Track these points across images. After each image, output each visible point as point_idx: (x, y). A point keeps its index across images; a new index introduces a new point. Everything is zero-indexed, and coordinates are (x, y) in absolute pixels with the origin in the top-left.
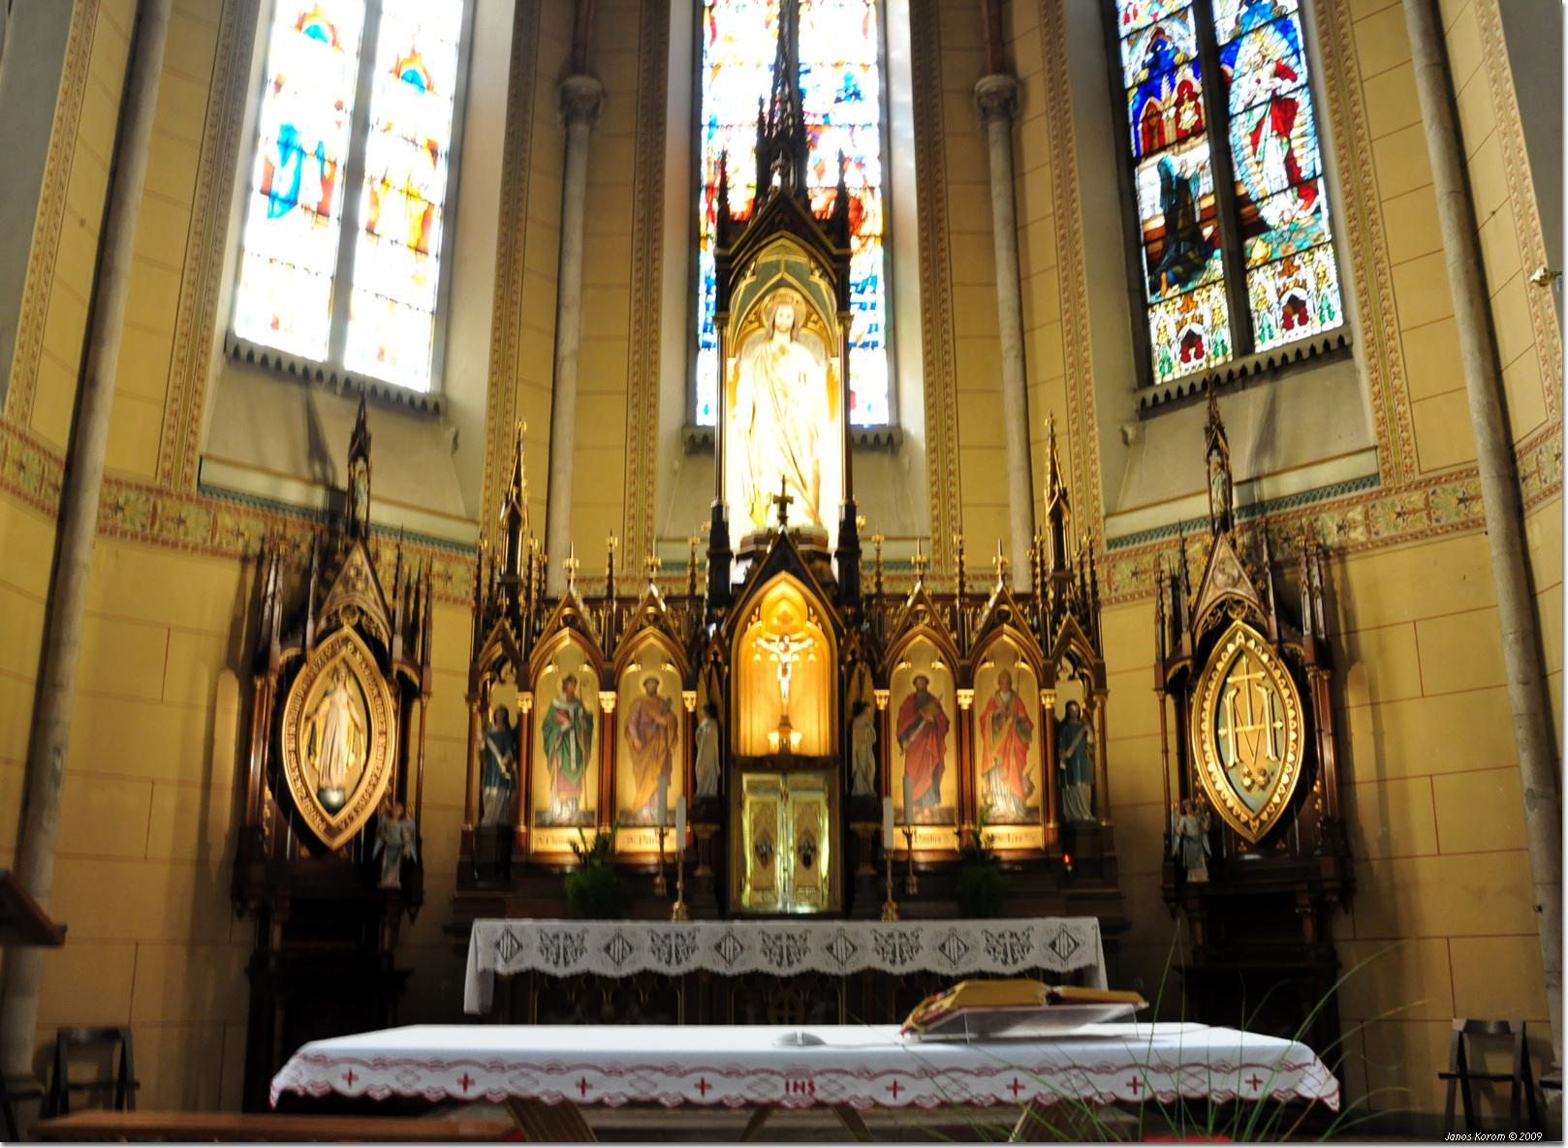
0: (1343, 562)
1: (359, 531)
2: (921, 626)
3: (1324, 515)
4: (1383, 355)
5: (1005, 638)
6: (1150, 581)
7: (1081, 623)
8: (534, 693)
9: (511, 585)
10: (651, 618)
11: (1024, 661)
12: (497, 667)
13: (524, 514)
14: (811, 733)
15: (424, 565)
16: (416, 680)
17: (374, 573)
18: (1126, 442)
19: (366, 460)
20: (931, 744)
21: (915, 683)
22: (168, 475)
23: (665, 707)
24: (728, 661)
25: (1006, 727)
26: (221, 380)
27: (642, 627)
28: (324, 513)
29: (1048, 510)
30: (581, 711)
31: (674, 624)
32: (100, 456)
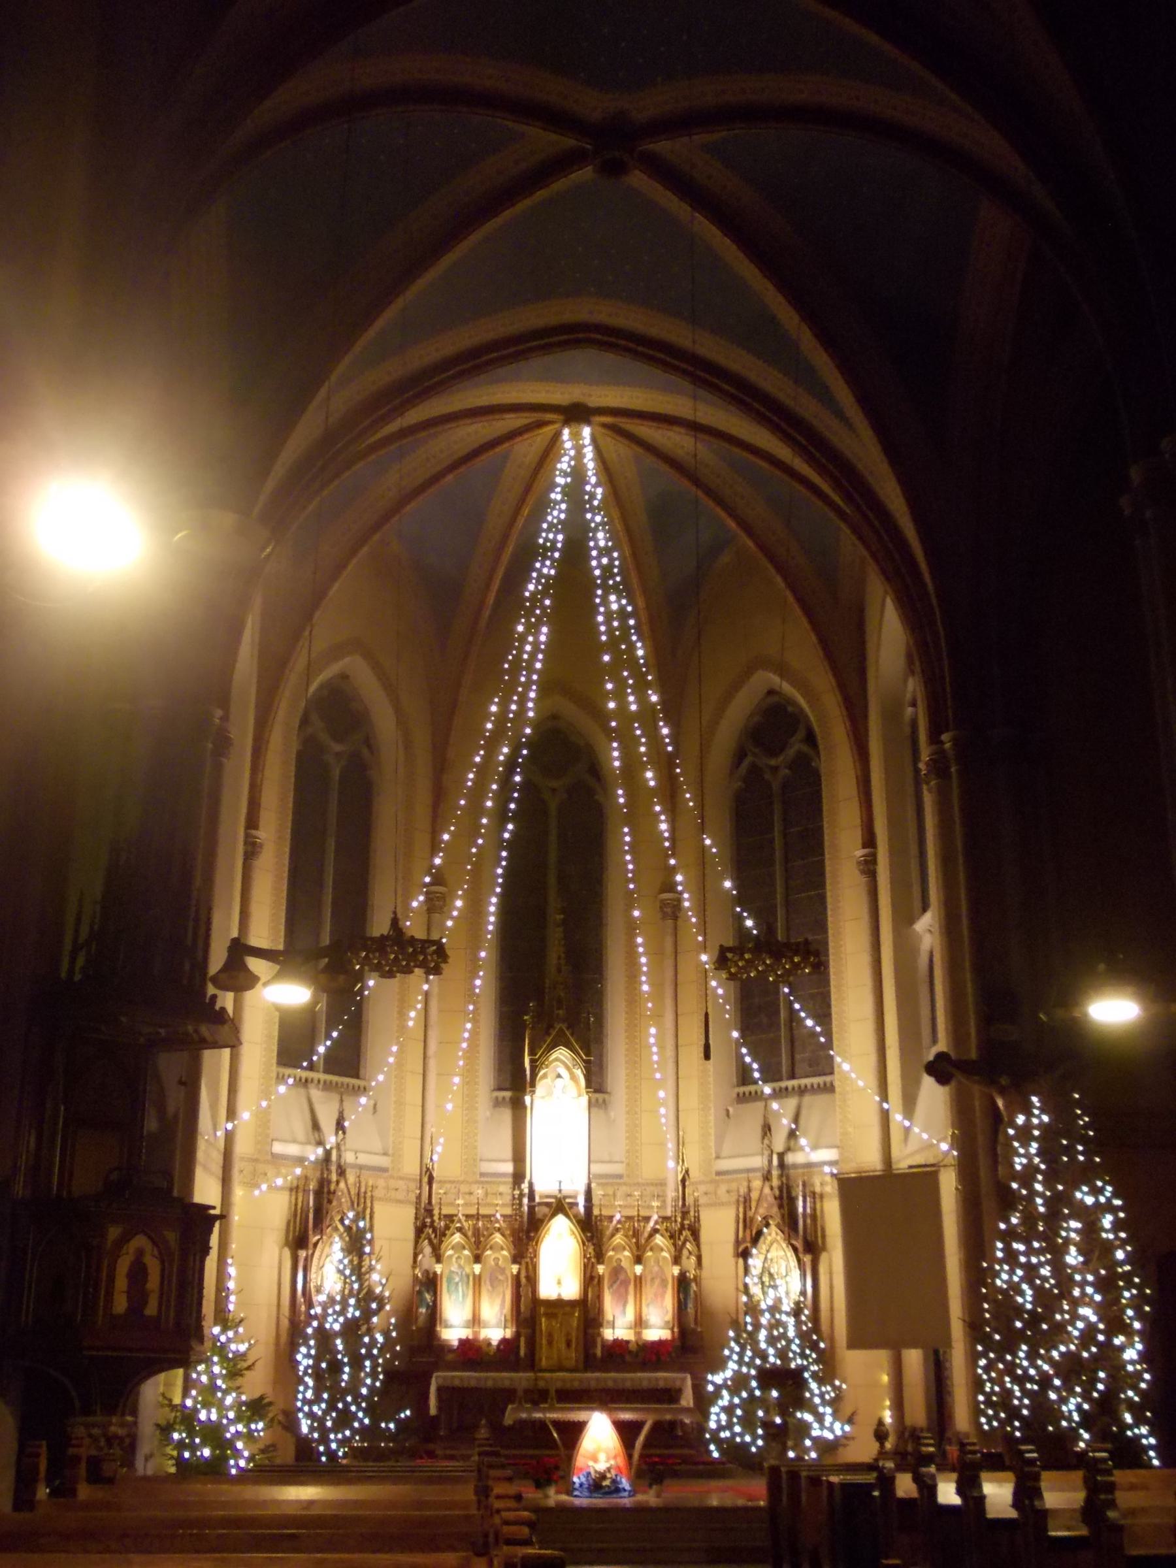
0: (822, 1201)
6: (734, 1198)
13: (435, 1175)
18: (728, 1115)
20: (622, 1290)
23: (502, 1271)
24: (535, 1256)
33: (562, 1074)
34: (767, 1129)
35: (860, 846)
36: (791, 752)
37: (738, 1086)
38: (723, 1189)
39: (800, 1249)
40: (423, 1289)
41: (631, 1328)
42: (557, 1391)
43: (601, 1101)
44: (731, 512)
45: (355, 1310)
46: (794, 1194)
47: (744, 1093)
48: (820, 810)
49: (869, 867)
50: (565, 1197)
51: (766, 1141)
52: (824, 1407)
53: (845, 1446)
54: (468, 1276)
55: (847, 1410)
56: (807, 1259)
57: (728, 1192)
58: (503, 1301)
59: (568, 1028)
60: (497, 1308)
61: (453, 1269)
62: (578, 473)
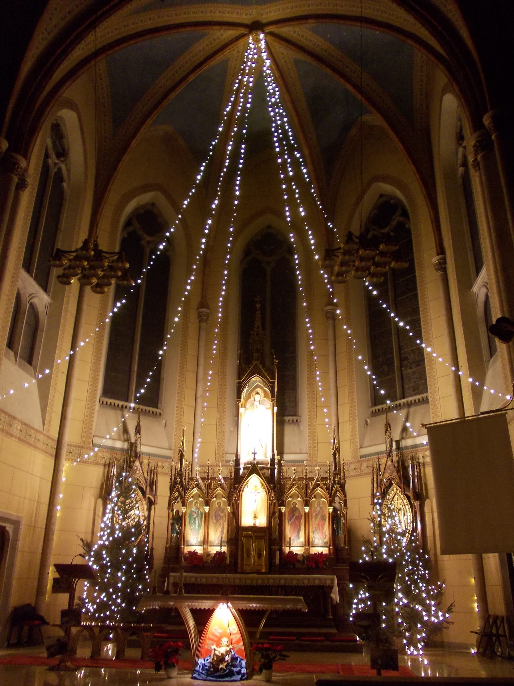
0: (424, 467)
1: (137, 456)
2: (294, 488)
3: (419, 453)
4: (435, 405)
5: (318, 491)
7: (340, 487)
8: (186, 506)
9: (180, 474)
10: (219, 485)
11: (324, 498)
12: (176, 499)
13: (184, 454)
14: (262, 521)
15: (156, 463)
16: (153, 500)
17: (142, 467)
19: (140, 434)
21: (293, 504)
22: (84, 442)
25: (318, 518)
26: (98, 411)
27: (217, 488)
28: (128, 450)
29: (332, 453)
30: (199, 512)
31: (225, 486)
32: (67, 438)
33: (259, 392)
34: (388, 426)
35: (436, 254)
36: (394, 223)
37: (372, 407)
38: (365, 465)
39: (412, 497)
40: (175, 522)
41: (302, 546)
42: (185, 585)
43: (295, 421)
44: (348, 80)
45: (119, 532)
46: (406, 465)
47: (376, 411)
48: (412, 249)
49: (442, 266)
50: (258, 463)
51: (388, 434)
52: (430, 600)
53: (447, 628)
54: (202, 514)
55: (447, 601)
56: (417, 503)
57: (367, 467)
58: (223, 528)
59: (260, 364)
60: (219, 533)
61: (192, 509)
62: (260, 62)
